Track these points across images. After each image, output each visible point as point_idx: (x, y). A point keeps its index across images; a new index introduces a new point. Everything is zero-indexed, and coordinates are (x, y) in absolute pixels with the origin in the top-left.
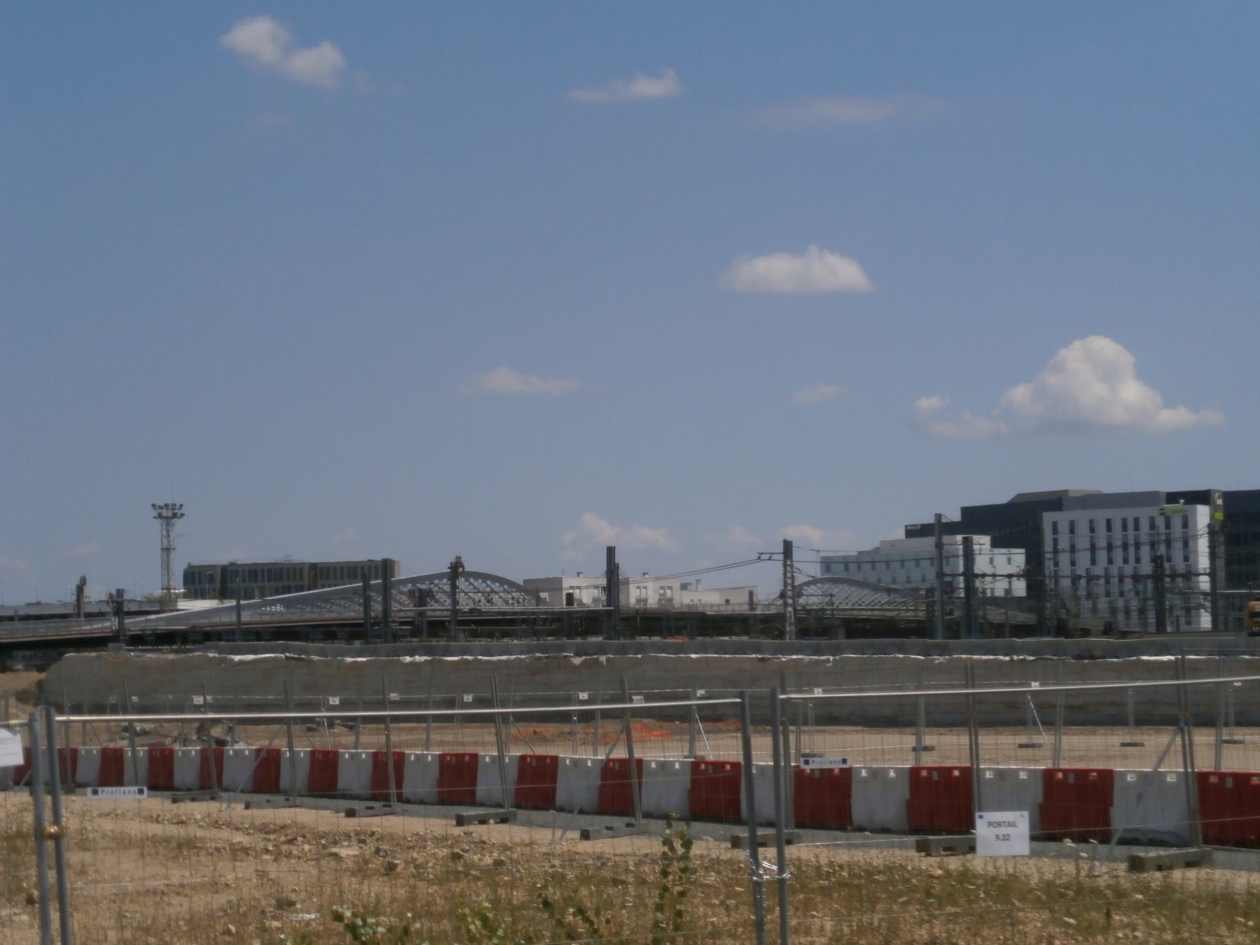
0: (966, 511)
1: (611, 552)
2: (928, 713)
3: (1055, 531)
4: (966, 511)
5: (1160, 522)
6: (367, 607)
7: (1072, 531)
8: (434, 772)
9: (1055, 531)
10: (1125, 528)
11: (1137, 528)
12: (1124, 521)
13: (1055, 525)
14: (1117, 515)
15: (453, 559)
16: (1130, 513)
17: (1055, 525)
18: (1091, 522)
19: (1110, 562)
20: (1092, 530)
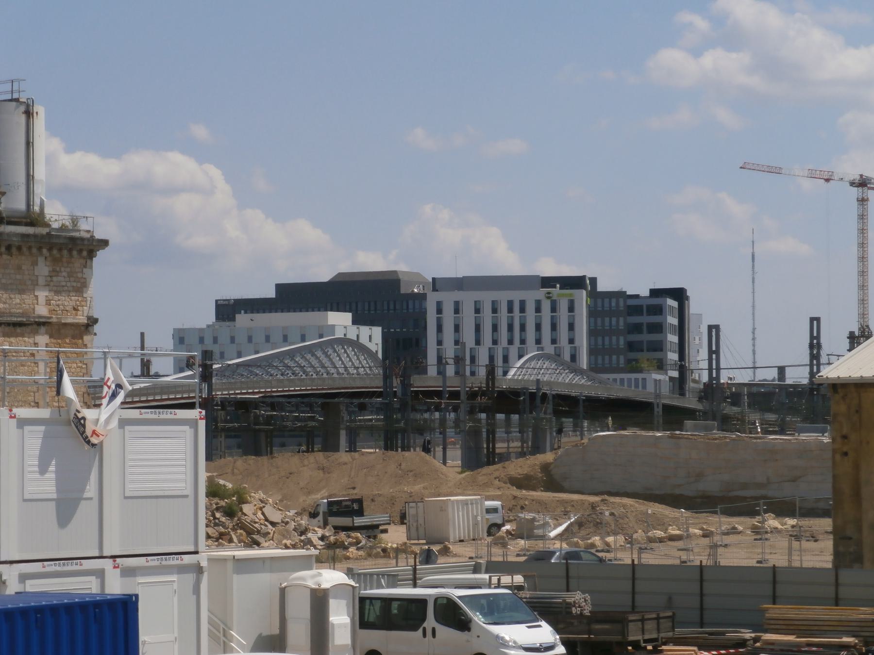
0: (279, 287)
1: (815, 321)
2: (800, 508)
3: (439, 311)
4: (279, 287)
5: (546, 306)
6: (499, 580)
7: (457, 311)
8: (326, 505)
9: (439, 311)
10: (510, 310)
11: (522, 310)
12: (510, 304)
13: (439, 305)
14: (503, 296)
15: (847, 334)
16: (516, 296)
17: (439, 305)
18: (493, 302)
19: (495, 342)
20: (477, 311)
